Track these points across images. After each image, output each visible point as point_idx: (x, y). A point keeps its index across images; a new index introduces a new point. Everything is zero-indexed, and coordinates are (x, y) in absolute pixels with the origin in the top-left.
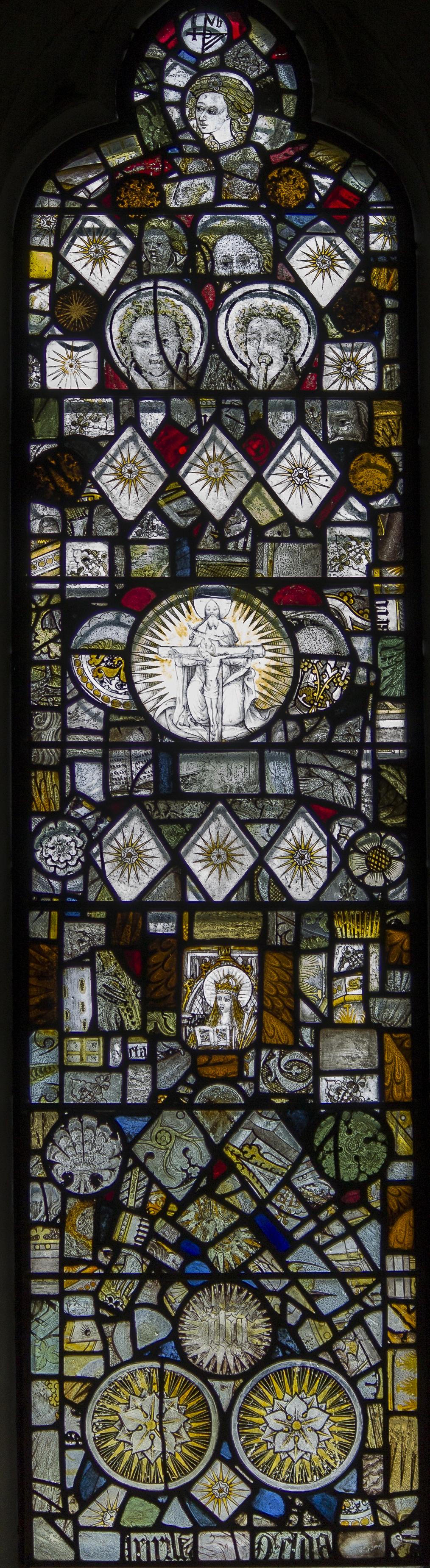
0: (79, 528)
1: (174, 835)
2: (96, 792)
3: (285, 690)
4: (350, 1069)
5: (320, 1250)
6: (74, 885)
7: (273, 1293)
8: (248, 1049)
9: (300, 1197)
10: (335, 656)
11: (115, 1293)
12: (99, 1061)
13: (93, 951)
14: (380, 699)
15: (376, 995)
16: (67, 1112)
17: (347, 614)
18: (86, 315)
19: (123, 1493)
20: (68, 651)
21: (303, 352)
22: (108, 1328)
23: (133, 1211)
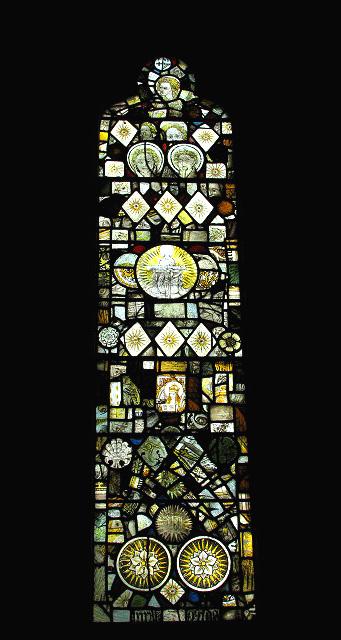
0: (117, 224)
1: (153, 332)
2: (123, 318)
3: (194, 281)
4: (222, 420)
5: (212, 491)
6: (115, 351)
7: (194, 508)
8: (182, 413)
9: (204, 470)
10: (213, 270)
11: (128, 508)
12: (123, 417)
13: (122, 375)
14: (230, 285)
15: (232, 393)
16: (111, 436)
17: (217, 255)
18: (119, 152)
19: (131, 593)
20: (113, 267)
21: (199, 167)
22: (126, 523)
23: (137, 475)
